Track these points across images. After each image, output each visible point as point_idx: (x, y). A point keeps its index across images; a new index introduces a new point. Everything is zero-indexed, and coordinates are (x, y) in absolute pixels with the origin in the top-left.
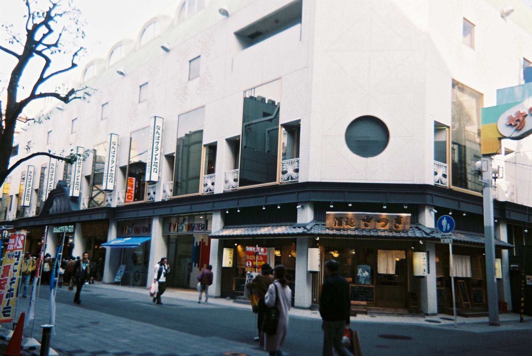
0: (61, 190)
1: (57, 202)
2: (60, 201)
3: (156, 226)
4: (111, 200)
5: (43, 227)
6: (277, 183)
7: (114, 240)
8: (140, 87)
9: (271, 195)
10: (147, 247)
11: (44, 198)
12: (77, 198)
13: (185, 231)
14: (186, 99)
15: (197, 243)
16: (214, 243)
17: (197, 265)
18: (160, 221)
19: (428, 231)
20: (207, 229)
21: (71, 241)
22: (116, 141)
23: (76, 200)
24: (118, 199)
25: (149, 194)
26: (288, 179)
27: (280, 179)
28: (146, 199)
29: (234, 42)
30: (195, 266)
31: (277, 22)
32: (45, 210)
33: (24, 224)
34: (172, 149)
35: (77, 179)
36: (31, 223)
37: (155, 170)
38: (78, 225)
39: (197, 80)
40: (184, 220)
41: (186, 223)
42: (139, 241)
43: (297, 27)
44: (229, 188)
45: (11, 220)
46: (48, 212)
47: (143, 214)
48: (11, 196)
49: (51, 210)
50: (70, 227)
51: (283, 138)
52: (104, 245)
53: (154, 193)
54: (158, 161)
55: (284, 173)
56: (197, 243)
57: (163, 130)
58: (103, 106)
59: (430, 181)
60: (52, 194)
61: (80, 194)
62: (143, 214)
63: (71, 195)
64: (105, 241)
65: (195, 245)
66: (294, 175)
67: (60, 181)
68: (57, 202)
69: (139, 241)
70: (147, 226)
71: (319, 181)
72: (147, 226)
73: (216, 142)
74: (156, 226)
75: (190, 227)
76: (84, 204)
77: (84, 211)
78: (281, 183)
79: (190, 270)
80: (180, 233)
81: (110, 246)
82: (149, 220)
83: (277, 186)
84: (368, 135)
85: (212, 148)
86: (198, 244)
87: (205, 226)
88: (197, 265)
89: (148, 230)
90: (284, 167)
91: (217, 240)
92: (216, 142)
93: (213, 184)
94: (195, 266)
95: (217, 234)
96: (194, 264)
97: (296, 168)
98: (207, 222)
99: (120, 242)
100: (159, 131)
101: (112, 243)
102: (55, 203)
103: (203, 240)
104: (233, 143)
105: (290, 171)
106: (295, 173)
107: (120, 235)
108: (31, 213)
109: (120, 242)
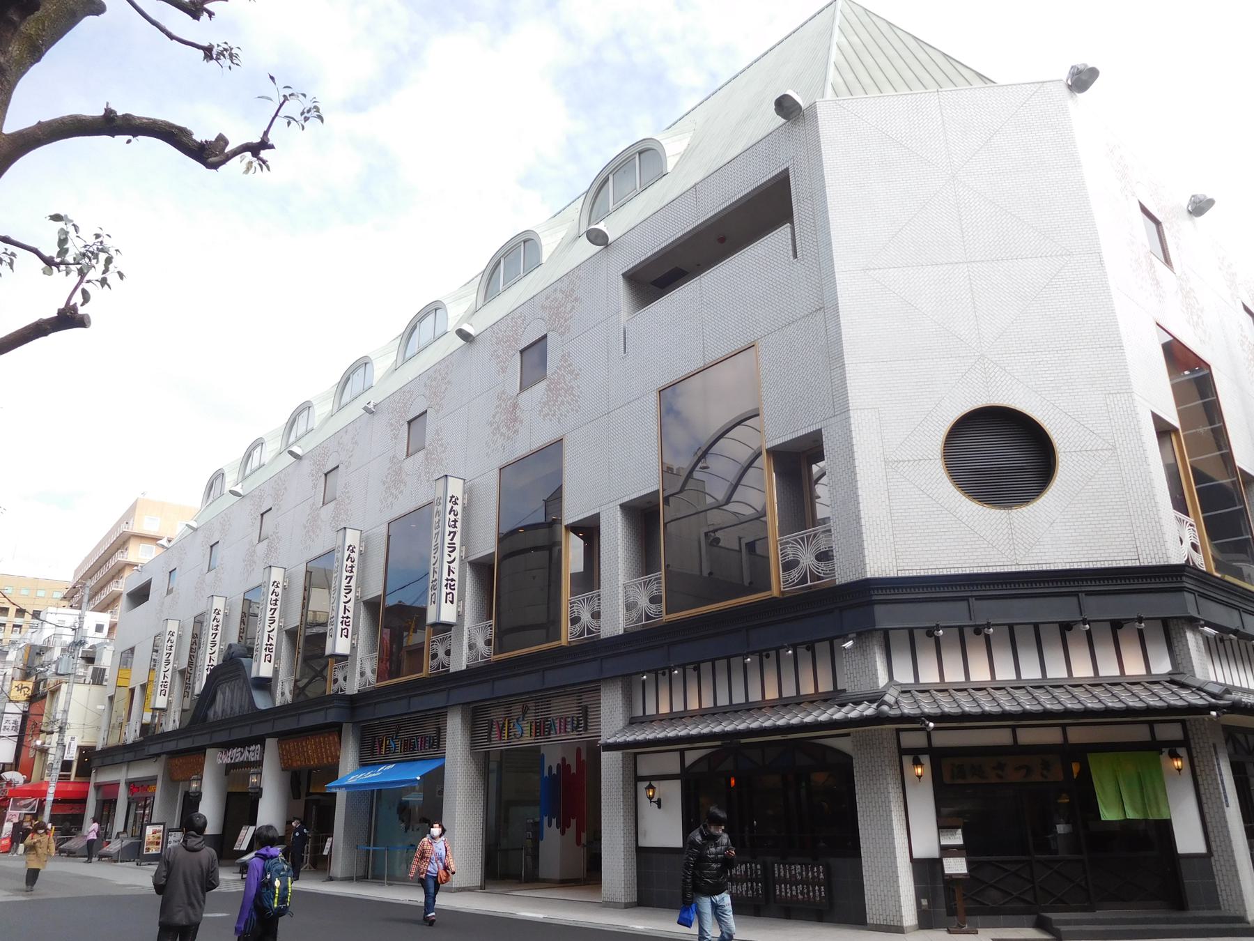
0: (233, 665)
1: (224, 694)
2: (232, 692)
3: (455, 732)
4: (345, 679)
5: (201, 751)
6: (423, 674)
7: (353, 774)
8: (409, 423)
9: (499, 679)
10: (434, 783)
11: (199, 685)
12: (268, 680)
13: (527, 740)
14: (516, 431)
15: (550, 768)
16: (611, 763)
17: (554, 821)
18: (463, 718)
19: (1216, 690)
20: (586, 729)
21: (254, 780)
22: (459, 494)
23: (264, 684)
24: (360, 675)
25: (435, 656)
26: (582, 634)
27: (567, 634)
28: (567, 634)
29: (621, 293)
30: (550, 825)
31: (722, 240)
32: (199, 711)
33: (154, 749)
34: (487, 545)
35: (449, 570)
36: (172, 746)
37: (345, 632)
38: (271, 743)
39: (421, 454)
40: (525, 712)
41: (531, 716)
42: (415, 773)
43: (783, 232)
44: (640, 619)
45: (130, 741)
46: (206, 716)
47: (420, 703)
48: (589, 531)
49: (211, 714)
50: (252, 748)
51: (573, 550)
52: (331, 786)
53: (448, 653)
54: (350, 614)
55: (789, 566)
56: (550, 768)
57: (464, 508)
58: (522, 352)
59: (1177, 554)
60: (216, 676)
61: (276, 671)
62: (420, 703)
63: (253, 675)
64: (334, 776)
65: (546, 773)
66: (592, 624)
67: (230, 646)
68: (224, 694)
69: (415, 773)
70: (431, 732)
71: (893, 574)
72: (431, 732)
73: (597, 517)
74: (455, 732)
75: (542, 728)
76: (283, 694)
77: (285, 708)
78: (783, 593)
79: (537, 835)
80: (516, 743)
81: (347, 787)
82: (440, 715)
83: (774, 600)
84: (1003, 452)
85: (589, 531)
86: (554, 771)
87: (586, 717)
88: (554, 821)
89: (437, 742)
90: (575, 609)
91: (618, 755)
92: (597, 517)
93: (345, 679)
94: (550, 825)
95: (611, 741)
96: (546, 819)
97: (596, 609)
98: (585, 711)
99: (370, 776)
100: (455, 507)
101: (351, 780)
102: (219, 697)
103: (564, 760)
104: (642, 515)
105: (807, 559)
106: (653, 606)
107: (366, 762)
108: (171, 723)
109: (370, 776)
